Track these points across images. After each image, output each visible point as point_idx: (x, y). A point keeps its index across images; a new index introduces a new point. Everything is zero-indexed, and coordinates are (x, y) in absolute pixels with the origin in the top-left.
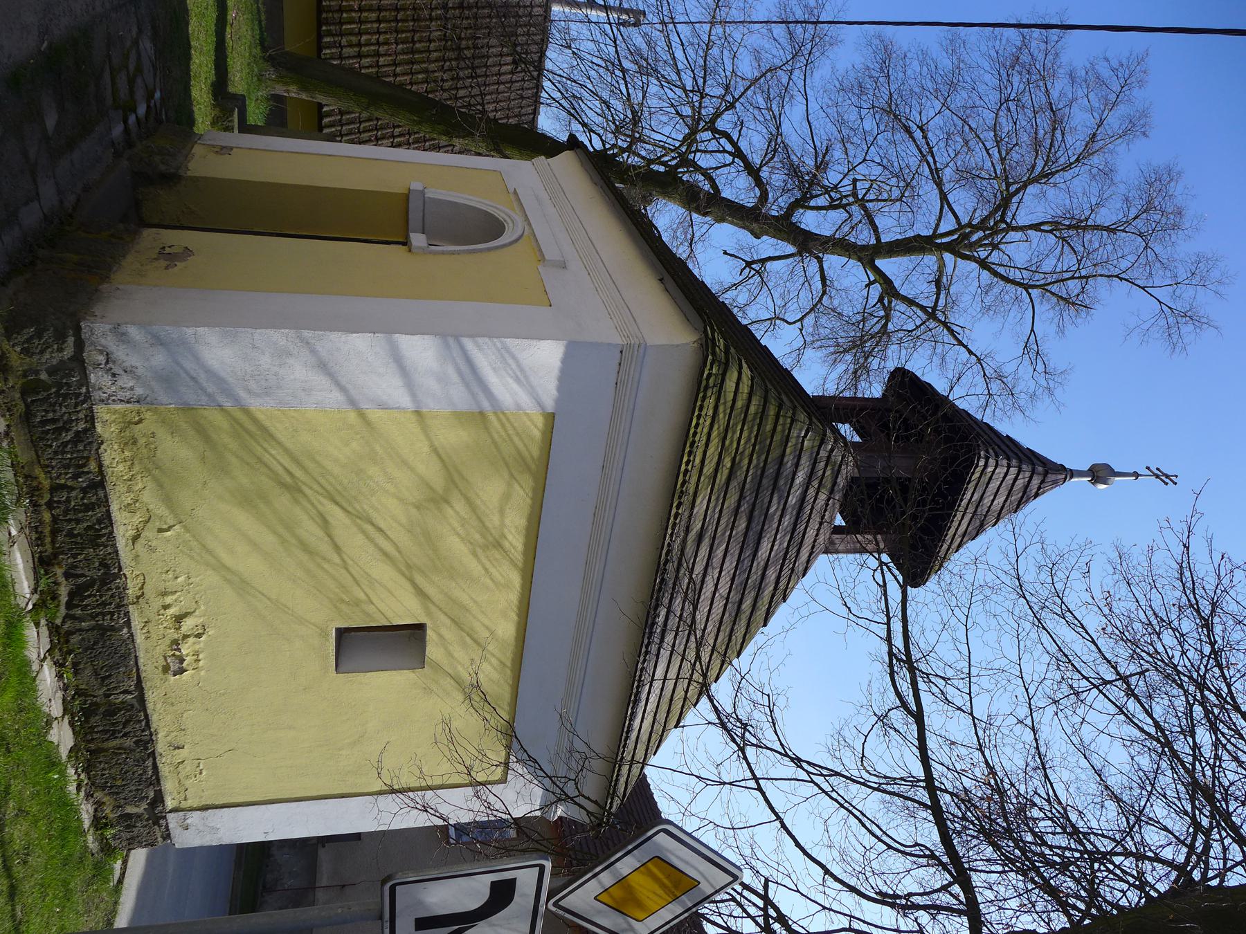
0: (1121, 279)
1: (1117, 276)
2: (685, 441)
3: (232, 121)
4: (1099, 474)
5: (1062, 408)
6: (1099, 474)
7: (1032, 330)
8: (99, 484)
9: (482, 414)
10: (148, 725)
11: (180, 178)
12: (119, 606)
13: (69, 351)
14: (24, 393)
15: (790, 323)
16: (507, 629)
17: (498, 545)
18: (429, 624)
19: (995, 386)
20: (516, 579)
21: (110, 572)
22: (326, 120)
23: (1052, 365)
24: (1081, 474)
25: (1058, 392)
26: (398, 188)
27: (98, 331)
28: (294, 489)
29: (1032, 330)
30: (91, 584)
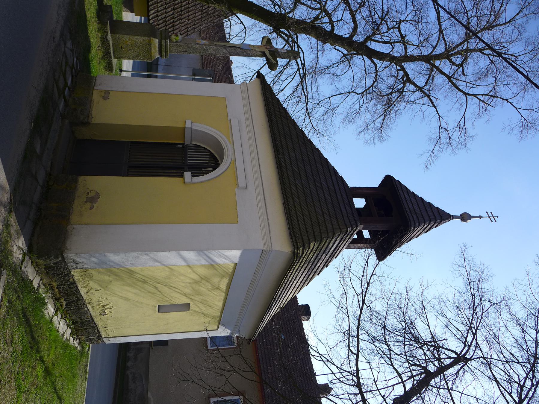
0: (508, 102)
1: (507, 100)
2: (292, 240)
3: (107, 29)
4: (465, 217)
5: (468, 151)
6: (465, 217)
7: (464, 115)
8: (74, 283)
9: (212, 265)
10: (95, 324)
11: (90, 123)
12: (83, 305)
13: (60, 259)
14: (45, 269)
15: (358, 94)
16: (220, 304)
17: (218, 288)
18: (191, 303)
19: (444, 136)
20: (223, 295)
21: (80, 298)
22: (150, 8)
23: (468, 132)
24: (457, 217)
25: (469, 144)
26: (181, 125)
27: (70, 256)
28: (145, 282)
29: (464, 115)
30: (74, 301)
